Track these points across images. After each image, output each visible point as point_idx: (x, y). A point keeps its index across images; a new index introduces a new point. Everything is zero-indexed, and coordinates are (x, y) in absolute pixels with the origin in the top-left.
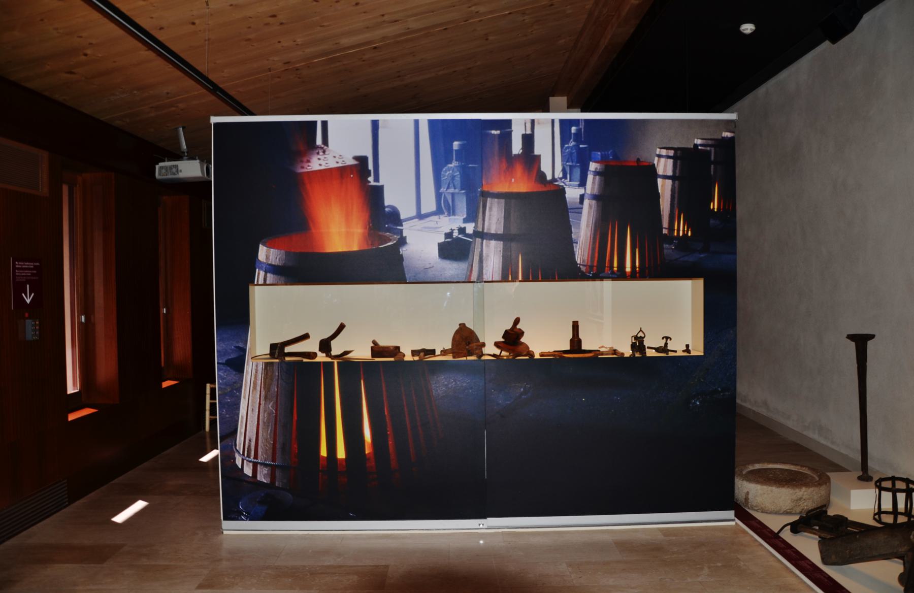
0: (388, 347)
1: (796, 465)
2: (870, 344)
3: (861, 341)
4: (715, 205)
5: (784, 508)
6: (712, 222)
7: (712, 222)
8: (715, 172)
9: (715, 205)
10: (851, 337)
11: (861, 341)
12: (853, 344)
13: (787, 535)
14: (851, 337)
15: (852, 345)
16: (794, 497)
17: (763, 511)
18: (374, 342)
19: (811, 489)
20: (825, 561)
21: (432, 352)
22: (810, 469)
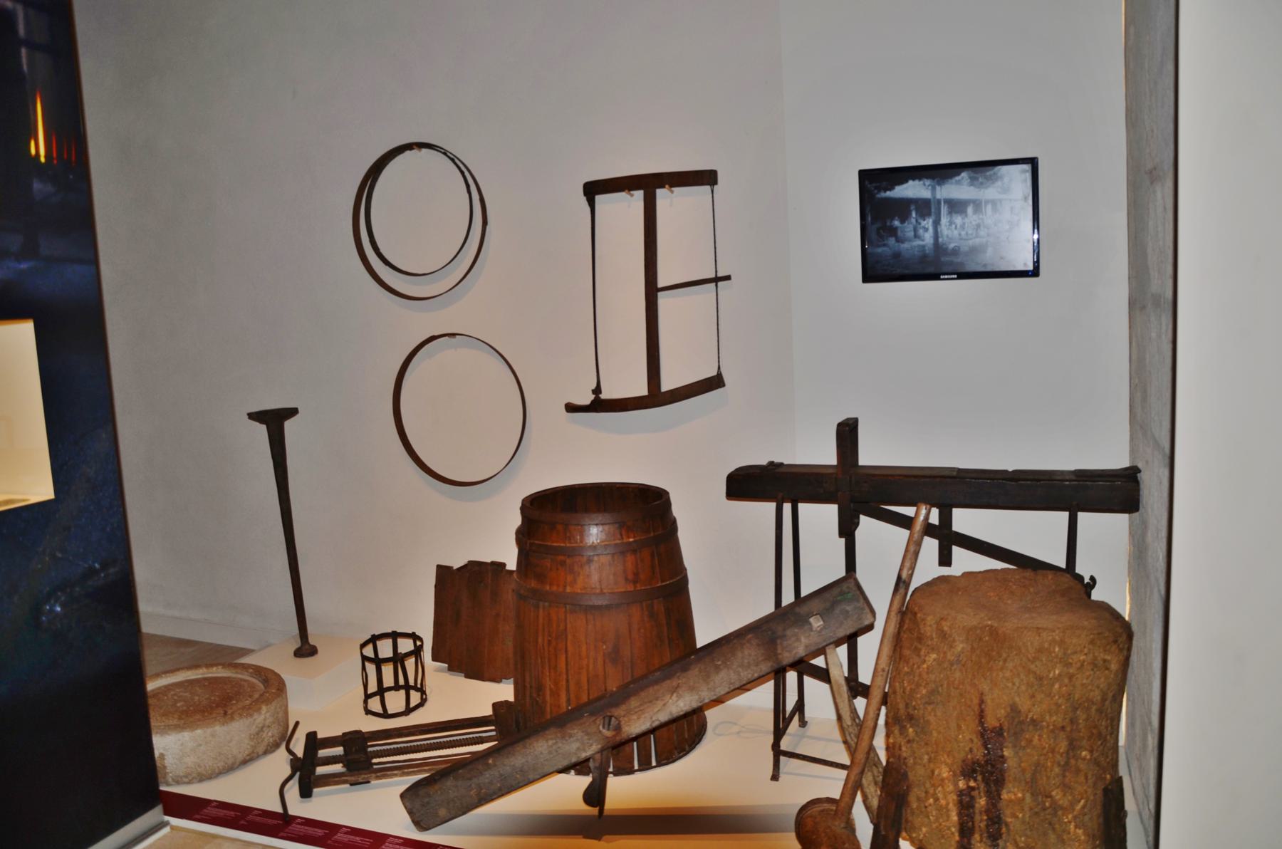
0: (1062, 472)
1: (197, 667)
2: (289, 425)
3: (274, 421)
4: (39, 147)
5: (240, 757)
6: (37, 186)
7: (37, 186)
8: (30, 64)
9: (39, 147)
10: (257, 416)
11: (274, 421)
12: (264, 427)
13: (298, 808)
14: (257, 416)
15: (262, 430)
16: (254, 730)
17: (202, 778)
18: (293, 412)
19: (274, 704)
20: (420, 825)
21: (92, 572)
22: (224, 665)
